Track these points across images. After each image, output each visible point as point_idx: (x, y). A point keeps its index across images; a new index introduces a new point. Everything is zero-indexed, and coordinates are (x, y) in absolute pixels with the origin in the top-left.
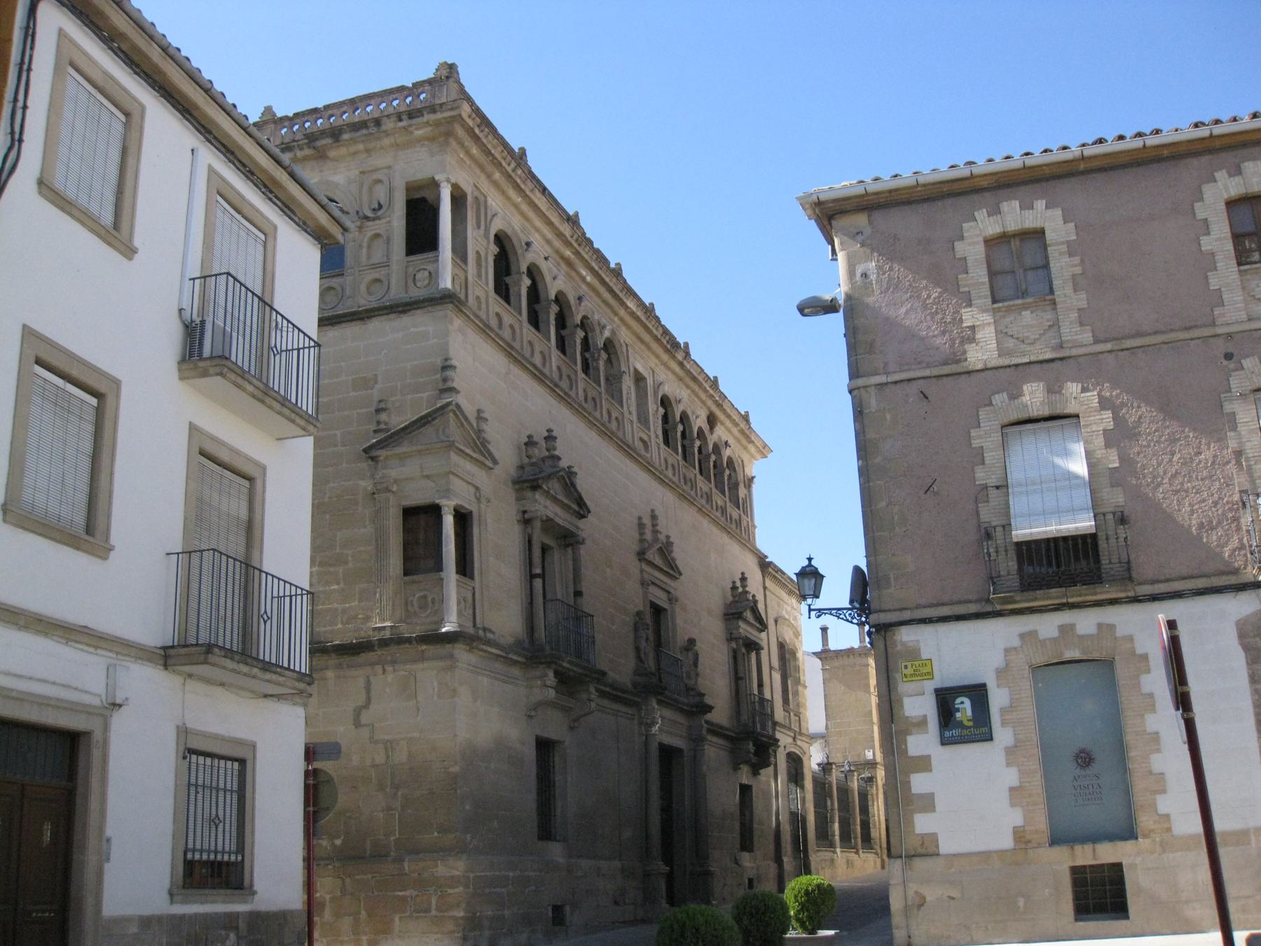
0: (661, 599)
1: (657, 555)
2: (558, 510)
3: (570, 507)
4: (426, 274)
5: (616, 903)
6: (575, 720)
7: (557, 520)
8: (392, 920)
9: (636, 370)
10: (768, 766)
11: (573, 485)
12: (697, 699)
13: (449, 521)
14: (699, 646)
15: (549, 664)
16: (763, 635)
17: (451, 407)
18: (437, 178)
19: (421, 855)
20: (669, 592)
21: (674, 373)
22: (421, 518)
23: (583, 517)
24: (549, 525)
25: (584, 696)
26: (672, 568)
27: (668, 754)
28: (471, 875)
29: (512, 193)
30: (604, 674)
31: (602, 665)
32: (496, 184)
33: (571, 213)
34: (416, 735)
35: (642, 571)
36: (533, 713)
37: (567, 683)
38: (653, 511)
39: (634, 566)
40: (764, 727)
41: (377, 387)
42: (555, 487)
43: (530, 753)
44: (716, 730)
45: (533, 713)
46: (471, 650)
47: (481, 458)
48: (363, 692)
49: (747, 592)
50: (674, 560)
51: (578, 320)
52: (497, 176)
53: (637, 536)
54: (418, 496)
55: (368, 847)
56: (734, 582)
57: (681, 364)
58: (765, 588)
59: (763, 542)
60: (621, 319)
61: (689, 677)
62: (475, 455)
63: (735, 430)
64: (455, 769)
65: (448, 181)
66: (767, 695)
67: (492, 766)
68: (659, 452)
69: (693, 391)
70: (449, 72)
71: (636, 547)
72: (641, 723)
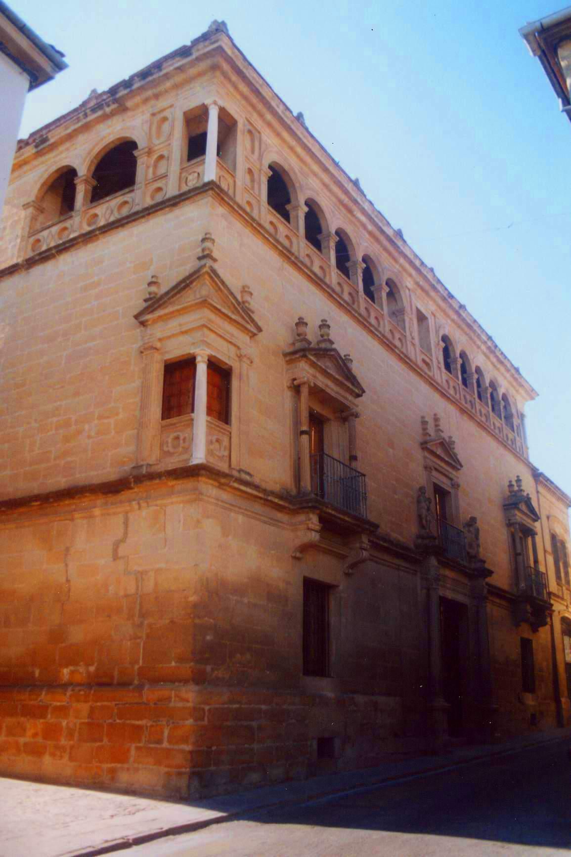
0: (445, 484)
1: (441, 452)
2: (330, 383)
4: (196, 175)
6: (353, 566)
8: (129, 750)
9: (418, 310)
10: (545, 624)
11: (349, 370)
13: (202, 371)
14: (479, 524)
15: (313, 508)
16: (537, 524)
17: (205, 270)
18: (206, 103)
19: (177, 684)
20: (451, 479)
22: (178, 372)
24: (317, 393)
26: (450, 456)
27: (451, 609)
28: (207, 708)
29: (286, 135)
31: (372, 517)
32: (269, 125)
34: (162, 565)
35: (425, 457)
38: (435, 415)
39: (419, 455)
40: (540, 593)
43: (296, 593)
44: (497, 592)
46: (221, 486)
47: (243, 322)
49: (521, 490)
50: (455, 455)
53: (421, 431)
54: (176, 350)
55: (116, 674)
56: (510, 482)
58: (538, 492)
59: (535, 459)
60: (401, 266)
61: (471, 546)
62: (233, 317)
63: (508, 375)
64: (193, 598)
65: (215, 103)
66: (542, 569)
67: (246, 600)
68: (440, 375)
70: (219, 28)
71: (419, 438)
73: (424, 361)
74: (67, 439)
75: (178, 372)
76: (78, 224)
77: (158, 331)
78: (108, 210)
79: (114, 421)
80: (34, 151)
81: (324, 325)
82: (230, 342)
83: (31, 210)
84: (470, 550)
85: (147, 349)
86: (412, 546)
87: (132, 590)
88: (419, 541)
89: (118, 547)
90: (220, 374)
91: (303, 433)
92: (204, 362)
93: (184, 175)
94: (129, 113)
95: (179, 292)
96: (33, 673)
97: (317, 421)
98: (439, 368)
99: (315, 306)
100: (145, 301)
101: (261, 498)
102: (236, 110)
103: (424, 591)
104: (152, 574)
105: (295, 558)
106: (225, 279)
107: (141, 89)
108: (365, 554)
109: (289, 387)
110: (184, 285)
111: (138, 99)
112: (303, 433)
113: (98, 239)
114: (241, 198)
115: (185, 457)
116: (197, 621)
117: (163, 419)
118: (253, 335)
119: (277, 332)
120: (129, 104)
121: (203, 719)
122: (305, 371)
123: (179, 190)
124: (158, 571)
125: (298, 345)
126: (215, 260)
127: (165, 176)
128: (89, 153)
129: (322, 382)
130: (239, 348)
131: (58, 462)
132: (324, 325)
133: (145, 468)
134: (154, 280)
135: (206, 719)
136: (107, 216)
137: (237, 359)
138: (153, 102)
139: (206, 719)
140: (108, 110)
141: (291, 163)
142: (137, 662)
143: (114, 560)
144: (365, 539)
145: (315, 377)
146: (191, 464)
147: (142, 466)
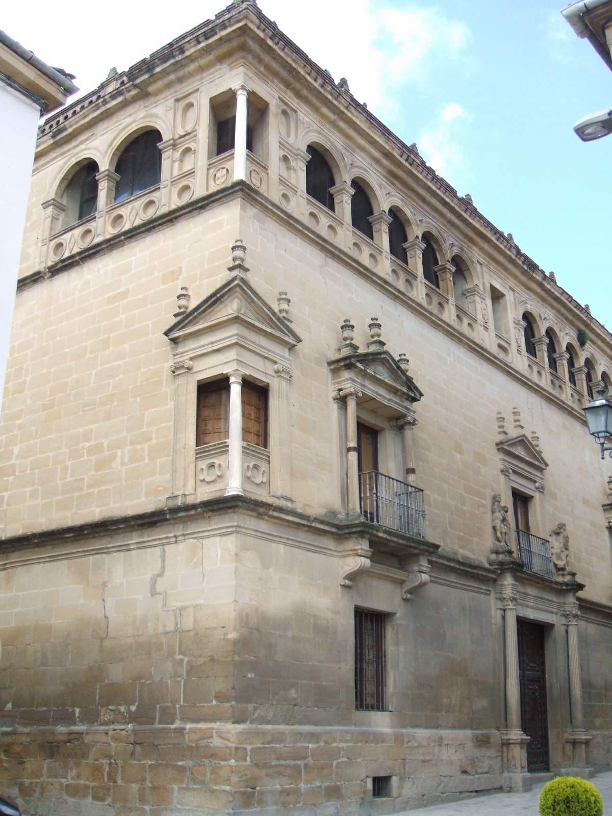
2: (383, 392)
3: (218, 293)
4: (225, 171)
5: (464, 772)
6: (410, 592)
7: (379, 399)
13: (236, 390)
15: (361, 534)
21: (536, 294)
22: (212, 391)
23: (414, 400)
24: (364, 402)
30: (437, 547)
31: (431, 536)
33: (409, 144)
34: (200, 601)
41: (181, 277)
43: (347, 624)
47: (278, 334)
48: (159, 561)
50: (540, 453)
54: (209, 369)
62: (269, 330)
64: (232, 636)
65: (243, 88)
68: (519, 361)
73: (500, 346)
74: (99, 466)
75: (212, 391)
76: (102, 227)
77: (190, 348)
78: (134, 212)
79: (148, 452)
80: (51, 141)
81: (375, 325)
82: (266, 358)
83: (50, 210)
84: (556, 562)
85: (178, 371)
87: (171, 627)
88: (493, 556)
89: (155, 582)
90: (257, 393)
91: (349, 450)
92: (238, 383)
93: (211, 171)
94: (152, 100)
95: (210, 306)
96: (74, 712)
97: (368, 434)
98: (519, 351)
99: (361, 303)
100: (176, 315)
101: (304, 525)
102: (269, 92)
103: (499, 613)
104: (191, 610)
105: (344, 586)
106: (258, 290)
107: (165, 73)
108: (425, 577)
110: (215, 299)
111: (159, 84)
112: (349, 450)
113: (123, 245)
114: (274, 194)
115: (218, 486)
116: (237, 658)
117: (197, 446)
118: (291, 348)
119: (319, 339)
120: (151, 89)
121: (245, 760)
122: (349, 382)
123: (207, 189)
124: (196, 607)
125: (346, 352)
126: (247, 270)
127: (191, 173)
128: (110, 146)
129: (371, 390)
130: (275, 363)
131: (91, 490)
132: (375, 325)
133: (180, 498)
134: (184, 292)
135: (248, 759)
136: (132, 218)
137: (274, 374)
138: (178, 87)
139: (248, 759)
140: (129, 95)
141: (333, 142)
142: (178, 700)
143: (152, 595)
144: (424, 563)
145: (363, 386)
146: (227, 494)
147: (177, 496)
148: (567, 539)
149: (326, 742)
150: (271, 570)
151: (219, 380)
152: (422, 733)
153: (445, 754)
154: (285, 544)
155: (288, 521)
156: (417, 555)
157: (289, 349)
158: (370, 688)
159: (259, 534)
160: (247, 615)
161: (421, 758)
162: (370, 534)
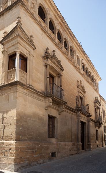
0: (82, 96)
5: (70, 151)
7: (54, 68)
12: (89, 114)
13: (18, 55)
16: (100, 107)
25: (62, 107)
27: (83, 123)
35: (78, 89)
36: (60, 114)
37: (55, 102)
42: (98, 102)
43: (46, 118)
44: (92, 120)
45: (60, 114)
47: (30, 44)
51: (86, 67)
52: (95, 72)
54: (11, 51)
57: (86, 57)
59: (100, 93)
61: (87, 110)
66: (101, 116)
69: (89, 64)
72: (77, 116)
75: (12, 58)
86: (75, 109)
91: (48, 77)
109: (44, 66)
112: (48, 77)
118: (34, 49)
119: (40, 51)
121: (19, 150)
135: (20, 150)
139: (20, 150)
148: (89, 107)
149: (41, 145)
150: (27, 103)
151: (13, 55)
152: (62, 143)
153: (66, 147)
154: (31, 97)
155: (31, 91)
156: (62, 104)
157: (33, 50)
158: (51, 133)
159: (24, 93)
160: (20, 113)
161: (62, 148)
162: (52, 97)
